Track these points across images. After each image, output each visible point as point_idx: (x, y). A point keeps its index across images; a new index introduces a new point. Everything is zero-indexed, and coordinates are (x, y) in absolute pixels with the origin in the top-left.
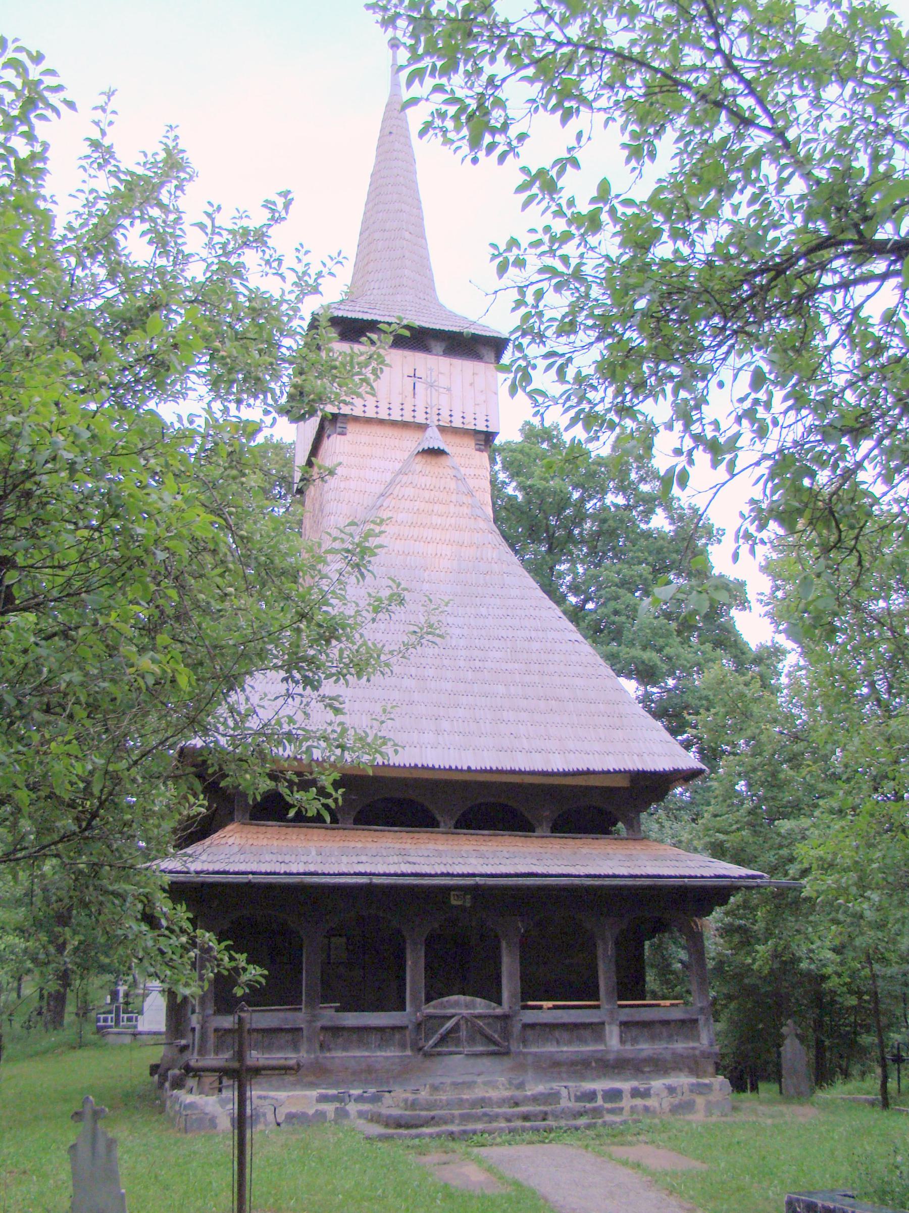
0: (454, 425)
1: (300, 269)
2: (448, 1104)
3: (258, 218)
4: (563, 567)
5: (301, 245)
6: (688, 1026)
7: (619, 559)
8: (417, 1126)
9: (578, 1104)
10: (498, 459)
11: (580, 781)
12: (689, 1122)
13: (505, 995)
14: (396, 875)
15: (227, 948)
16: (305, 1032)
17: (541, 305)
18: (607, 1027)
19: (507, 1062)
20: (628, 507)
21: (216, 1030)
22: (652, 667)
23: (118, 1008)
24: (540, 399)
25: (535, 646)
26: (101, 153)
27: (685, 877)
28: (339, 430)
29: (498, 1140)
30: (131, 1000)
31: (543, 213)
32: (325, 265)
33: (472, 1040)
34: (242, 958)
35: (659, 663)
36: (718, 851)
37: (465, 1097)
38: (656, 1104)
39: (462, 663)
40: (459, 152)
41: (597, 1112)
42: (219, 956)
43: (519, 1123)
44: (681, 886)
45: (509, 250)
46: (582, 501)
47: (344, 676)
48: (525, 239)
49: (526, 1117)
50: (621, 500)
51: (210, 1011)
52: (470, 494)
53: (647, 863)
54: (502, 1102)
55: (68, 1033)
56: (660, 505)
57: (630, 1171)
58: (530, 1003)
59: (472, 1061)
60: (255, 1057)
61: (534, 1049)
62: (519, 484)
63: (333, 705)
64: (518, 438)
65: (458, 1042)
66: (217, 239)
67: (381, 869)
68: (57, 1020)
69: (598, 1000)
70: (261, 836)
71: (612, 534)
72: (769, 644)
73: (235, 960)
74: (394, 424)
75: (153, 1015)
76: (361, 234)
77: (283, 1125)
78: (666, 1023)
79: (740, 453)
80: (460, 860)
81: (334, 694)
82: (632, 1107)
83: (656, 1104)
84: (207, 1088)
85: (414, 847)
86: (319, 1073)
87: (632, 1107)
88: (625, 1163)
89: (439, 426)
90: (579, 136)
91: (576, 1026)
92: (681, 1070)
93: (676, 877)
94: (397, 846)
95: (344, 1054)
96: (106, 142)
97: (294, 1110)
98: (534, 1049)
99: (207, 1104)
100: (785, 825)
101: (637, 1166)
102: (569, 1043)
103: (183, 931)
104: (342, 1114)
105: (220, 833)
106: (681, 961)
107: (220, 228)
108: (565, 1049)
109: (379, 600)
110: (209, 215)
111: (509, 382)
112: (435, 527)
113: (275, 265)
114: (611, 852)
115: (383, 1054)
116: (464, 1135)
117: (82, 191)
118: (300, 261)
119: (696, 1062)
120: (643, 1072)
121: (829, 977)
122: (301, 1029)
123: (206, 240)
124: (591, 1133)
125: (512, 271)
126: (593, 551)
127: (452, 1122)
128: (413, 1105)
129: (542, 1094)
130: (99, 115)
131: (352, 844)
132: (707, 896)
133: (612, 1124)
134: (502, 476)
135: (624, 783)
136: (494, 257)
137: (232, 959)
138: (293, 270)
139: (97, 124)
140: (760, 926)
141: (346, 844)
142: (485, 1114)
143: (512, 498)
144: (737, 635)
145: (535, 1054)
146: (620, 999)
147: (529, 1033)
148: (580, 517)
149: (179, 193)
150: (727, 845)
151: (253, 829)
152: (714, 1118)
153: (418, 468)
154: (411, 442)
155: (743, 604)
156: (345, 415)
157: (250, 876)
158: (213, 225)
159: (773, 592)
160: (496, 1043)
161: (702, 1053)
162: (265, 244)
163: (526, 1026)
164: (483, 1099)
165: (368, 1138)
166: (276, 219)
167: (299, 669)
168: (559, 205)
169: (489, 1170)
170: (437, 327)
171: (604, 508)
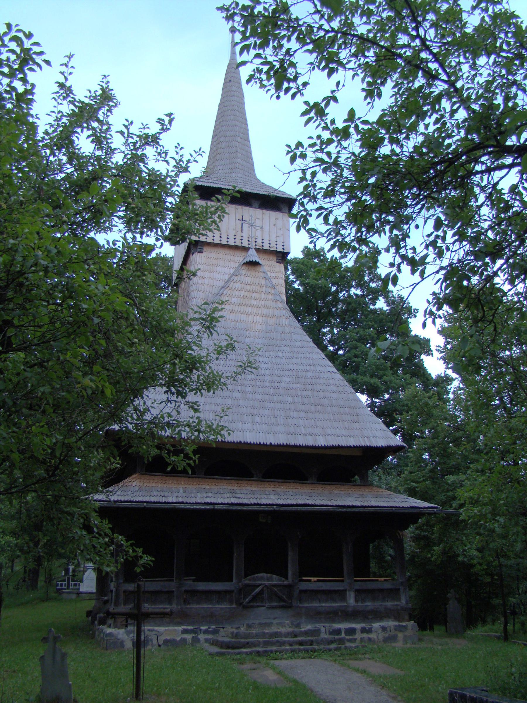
0: (264, 248)
3: (155, 128)
5: (179, 144)
6: (394, 593)
7: (358, 325)
8: (241, 648)
13: (290, 573)
14: (228, 504)
15: (132, 545)
16: (175, 593)
17: (315, 180)
18: (348, 592)
20: (363, 296)
21: (125, 592)
23: (69, 578)
24: (314, 234)
25: (309, 374)
27: (393, 507)
28: (199, 250)
29: (285, 656)
30: (76, 574)
31: (317, 127)
32: (192, 156)
34: (140, 551)
35: (380, 385)
36: (412, 493)
37: (266, 631)
38: (375, 637)
39: (267, 384)
41: (341, 641)
43: (296, 647)
45: (297, 148)
46: (337, 292)
47: (200, 390)
48: (306, 143)
49: (301, 643)
50: (359, 292)
53: (372, 499)
54: (287, 635)
56: (382, 295)
57: (360, 675)
58: (304, 578)
60: (147, 607)
61: (306, 605)
62: (301, 282)
63: (194, 407)
64: (301, 256)
66: (130, 140)
67: (220, 501)
68: (34, 585)
69: (343, 577)
70: (152, 481)
71: (354, 311)
72: (443, 375)
73: (136, 551)
74: (230, 247)
75: (89, 583)
76: (213, 138)
77: (162, 646)
78: (381, 590)
79: (427, 266)
80: (265, 496)
82: (361, 638)
83: (375, 637)
87: (361, 638)
88: (357, 670)
90: (338, 84)
92: (390, 618)
93: (388, 507)
94: (229, 488)
95: (198, 606)
96: (68, 84)
97: (168, 638)
98: (306, 605)
99: (119, 633)
100: (451, 479)
101: (364, 672)
102: (326, 601)
103: (106, 535)
104: (196, 640)
105: (128, 479)
106: (390, 555)
107: (132, 134)
108: (324, 605)
109: (221, 347)
110: (126, 127)
111: (296, 224)
112: (253, 306)
113: (163, 155)
114: (351, 493)
115: (220, 606)
116: (265, 653)
117: (54, 112)
118: (177, 153)
120: (368, 618)
122: (173, 592)
123: (124, 141)
126: (343, 321)
128: (237, 636)
129: (310, 630)
130: (64, 69)
131: (203, 487)
134: (291, 277)
135: (359, 454)
136: (288, 153)
137: (134, 551)
138: (173, 158)
139: (63, 73)
140: (436, 536)
141: (200, 486)
144: (425, 370)
145: (307, 607)
148: (336, 301)
149: (109, 114)
150: (417, 489)
152: (408, 645)
153: (244, 272)
154: (239, 258)
155: (429, 352)
156: (202, 242)
157: (145, 504)
159: (445, 346)
160: (284, 601)
162: (158, 143)
163: (301, 591)
165: (210, 654)
166: (164, 129)
167: (175, 386)
168: (326, 123)
169: (280, 673)
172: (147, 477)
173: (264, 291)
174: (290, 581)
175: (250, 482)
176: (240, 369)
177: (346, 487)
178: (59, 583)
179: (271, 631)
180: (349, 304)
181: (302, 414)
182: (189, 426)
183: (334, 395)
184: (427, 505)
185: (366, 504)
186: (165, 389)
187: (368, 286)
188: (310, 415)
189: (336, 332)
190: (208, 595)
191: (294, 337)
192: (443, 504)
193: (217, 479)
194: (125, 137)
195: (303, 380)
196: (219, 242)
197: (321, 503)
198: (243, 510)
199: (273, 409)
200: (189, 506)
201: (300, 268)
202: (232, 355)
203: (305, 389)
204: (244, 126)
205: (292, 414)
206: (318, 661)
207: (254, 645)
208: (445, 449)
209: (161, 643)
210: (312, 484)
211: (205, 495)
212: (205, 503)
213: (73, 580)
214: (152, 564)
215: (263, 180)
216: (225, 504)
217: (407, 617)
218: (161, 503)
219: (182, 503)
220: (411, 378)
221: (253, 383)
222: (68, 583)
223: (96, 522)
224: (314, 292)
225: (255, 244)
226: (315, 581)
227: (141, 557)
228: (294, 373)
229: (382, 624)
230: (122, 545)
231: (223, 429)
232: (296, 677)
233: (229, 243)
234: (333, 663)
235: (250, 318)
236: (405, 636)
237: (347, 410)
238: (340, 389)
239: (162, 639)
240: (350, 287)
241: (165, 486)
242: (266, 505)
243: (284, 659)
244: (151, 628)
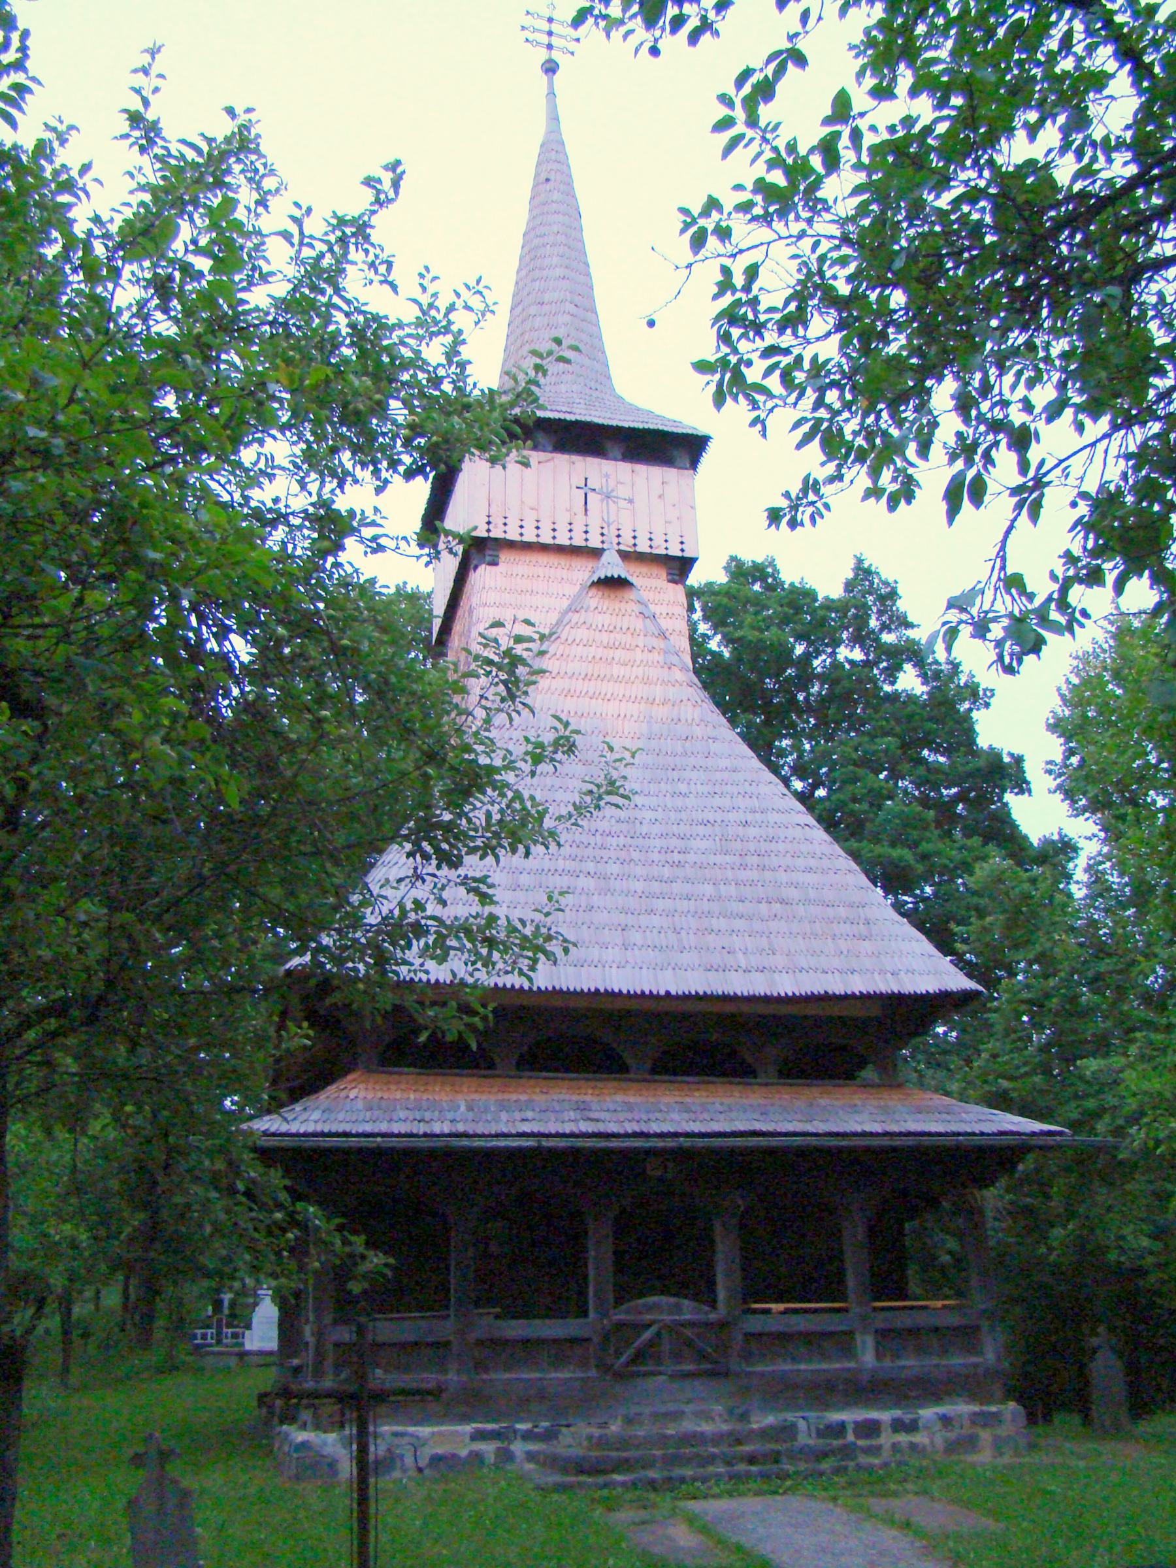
0: (639, 549)
1: (425, 300)
3: (356, 203)
4: (785, 743)
5: (427, 269)
6: (967, 1336)
7: (857, 731)
8: (605, 1472)
9: (821, 1441)
10: (697, 605)
11: (812, 1010)
12: (973, 1465)
13: (722, 1294)
14: (572, 1135)
15: (340, 1228)
17: (755, 288)
18: (858, 1337)
20: (867, 664)
21: (337, 1345)
22: (904, 869)
23: (220, 1321)
24: (760, 398)
25: (752, 832)
26: (143, 128)
27: (959, 1134)
28: (488, 559)
29: (716, 1490)
30: (238, 1312)
31: (753, 161)
32: (458, 295)
33: (677, 1357)
34: (359, 1241)
36: (1001, 1101)
39: (656, 856)
40: (630, 38)
41: (847, 1452)
42: (328, 1239)
43: (742, 1467)
45: (705, 213)
46: (807, 657)
47: (493, 849)
48: (730, 200)
49: (752, 1460)
50: (857, 655)
51: (328, 1319)
52: (663, 635)
55: (156, 1356)
56: (909, 660)
57: (895, 1533)
60: (380, 1377)
61: (760, 1368)
62: (724, 637)
63: (479, 889)
64: (722, 578)
65: (658, 1358)
66: (307, 252)
67: (552, 1128)
68: (145, 1339)
69: (844, 1299)
70: (393, 1087)
71: (846, 699)
72: (1056, 837)
73: (350, 1243)
74: (560, 550)
75: (263, 1330)
76: (512, 309)
77: (427, 1472)
79: (1046, 490)
80: (658, 1115)
81: (478, 875)
83: (926, 1441)
85: (595, 1099)
86: (470, 1403)
87: (894, 1444)
88: (889, 1521)
89: (619, 551)
90: (805, 16)
93: (946, 1134)
94: (575, 1098)
95: (507, 1376)
96: (150, 116)
97: (440, 1450)
98: (760, 1368)
99: (325, 1444)
100: (1091, 1065)
101: (907, 1525)
103: (280, 1206)
104: (506, 1456)
105: (341, 1084)
106: (950, 1253)
107: (311, 237)
109: (541, 745)
110: (294, 219)
111: (713, 388)
112: (618, 680)
113: (382, 269)
114: (859, 1103)
115: (560, 1375)
116: (670, 1484)
117: (129, 205)
118: (424, 289)
120: (907, 1397)
121: (1146, 1273)
122: (447, 1344)
123: (292, 252)
125: (712, 242)
126: (822, 723)
128: (601, 1442)
129: (771, 1427)
130: (140, 80)
131: (514, 1097)
133: (869, 1468)
134: (703, 628)
135: (875, 1011)
136: (686, 227)
137: (346, 1242)
138: (415, 301)
139: (138, 91)
140: (1056, 1204)
141: (506, 1096)
143: (717, 655)
144: (1014, 826)
145: (762, 1375)
146: (878, 1299)
148: (805, 678)
149: (260, 210)
150: (1014, 1095)
152: (1006, 1459)
153: (593, 603)
154: (582, 572)
155: (1022, 786)
156: (496, 539)
158: (301, 232)
159: (1067, 758)
161: (987, 1370)
162: (367, 238)
163: (749, 1336)
164: (694, 1435)
165: (538, 1488)
166: (380, 203)
167: (431, 841)
168: (775, 150)
169: (705, 1530)
170: (614, 423)
171: (836, 665)
172: (384, 1077)
173: (641, 644)
175: (623, 1084)
176: (588, 799)
178: (199, 1332)
180: (834, 682)
181: (739, 924)
182: (468, 932)
183: (810, 878)
184: (1037, 1126)
185: (894, 1128)
186: (408, 846)
187: (877, 640)
188: (758, 926)
189: (807, 747)
190: (529, 1347)
191: (714, 747)
192: (1075, 1125)
194: (292, 245)
195: (738, 845)
196: (535, 540)
199: (671, 914)
201: (721, 606)
202: (571, 766)
203: (743, 866)
204: (582, 279)
205: (715, 923)
206: (795, 1501)
207: (648, 1464)
208: (1074, 999)
209: (423, 1463)
210: (766, 1085)
211: (518, 1115)
213: (229, 1325)
214: (389, 1273)
215: (629, 398)
216: (564, 1135)
217: (998, 1390)
219: (465, 1135)
220: (985, 843)
221: (623, 855)
222: (219, 1333)
223: (252, 1174)
224: (757, 659)
225: (616, 540)
227: (363, 1257)
228: (717, 829)
230: (318, 1228)
231: (549, 938)
232: (743, 1541)
233: (557, 542)
234: (831, 1505)
235: (612, 708)
237: (842, 912)
238: (826, 863)
239: (427, 1452)
240: (836, 643)
241: (425, 1097)
243: (715, 1496)
244: (399, 1428)
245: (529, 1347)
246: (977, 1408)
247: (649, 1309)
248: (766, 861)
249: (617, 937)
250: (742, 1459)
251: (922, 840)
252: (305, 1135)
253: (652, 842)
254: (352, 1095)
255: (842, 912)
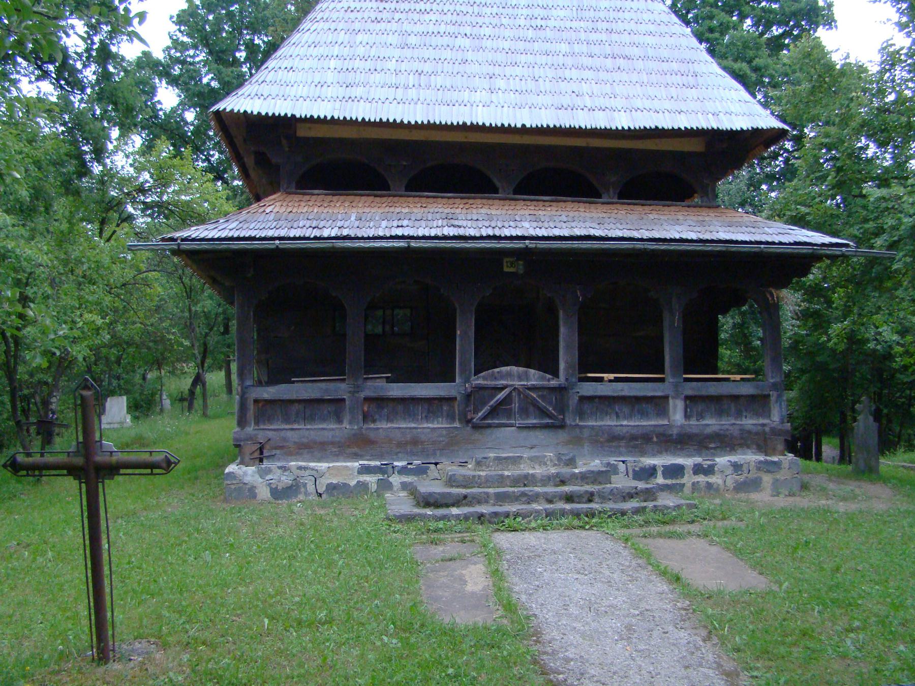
2: (487, 481)
6: (758, 403)
8: (447, 506)
13: (562, 366)
14: (436, 238)
16: (347, 403)
18: (671, 401)
19: (562, 435)
27: (761, 243)
29: (533, 525)
33: (524, 412)
35: (748, 72)
36: (800, 221)
37: (506, 473)
38: (720, 481)
39: (522, 22)
44: (755, 253)
49: (569, 498)
53: (720, 229)
54: (547, 480)
58: (590, 375)
59: (525, 433)
65: (509, 414)
77: (324, 496)
78: (735, 398)
80: (512, 224)
82: (693, 484)
83: (720, 481)
84: (247, 459)
85: (464, 211)
86: (358, 445)
87: (693, 484)
91: (638, 399)
92: (748, 447)
93: (751, 242)
95: (389, 425)
97: (335, 482)
99: (245, 474)
102: (629, 417)
104: (385, 485)
108: (625, 423)
114: (681, 218)
115: (430, 425)
119: (765, 440)
120: (707, 448)
122: (344, 400)
124: (639, 518)
127: (487, 502)
132: (787, 265)
141: (392, 209)
142: (524, 494)
145: (592, 427)
147: (586, 407)
151: (297, 198)
157: (277, 242)
160: (549, 416)
163: (583, 399)
164: (526, 476)
174: (562, 380)
175: (490, 202)
177: (672, 208)
179: (517, 472)
183: (649, 40)
184: (828, 239)
185: (708, 236)
188: (603, 75)
190: (408, 404)
192: (859, 241)
193: (428, 197)
197: (620, 234)
198: (466, 249)
200: (362, 244)
203: (595, 30)
205: (567, 74)
212: (392, 237)
217: (780, 447)
218: (308, 238)
226: (610, 381)
229: (734, 458)
236: (776, 481)
238: (663, 28)
242: (511, 238)
245: (408, 404)
246: (761, 458)
247: (502, 376)
248: (614, 26)
249: (486, 84)
250: (561, 499)
251: (756, 57)
252: (219, 239)
253: (520, 12)
254: (268, 210)
255: (675, 66)
